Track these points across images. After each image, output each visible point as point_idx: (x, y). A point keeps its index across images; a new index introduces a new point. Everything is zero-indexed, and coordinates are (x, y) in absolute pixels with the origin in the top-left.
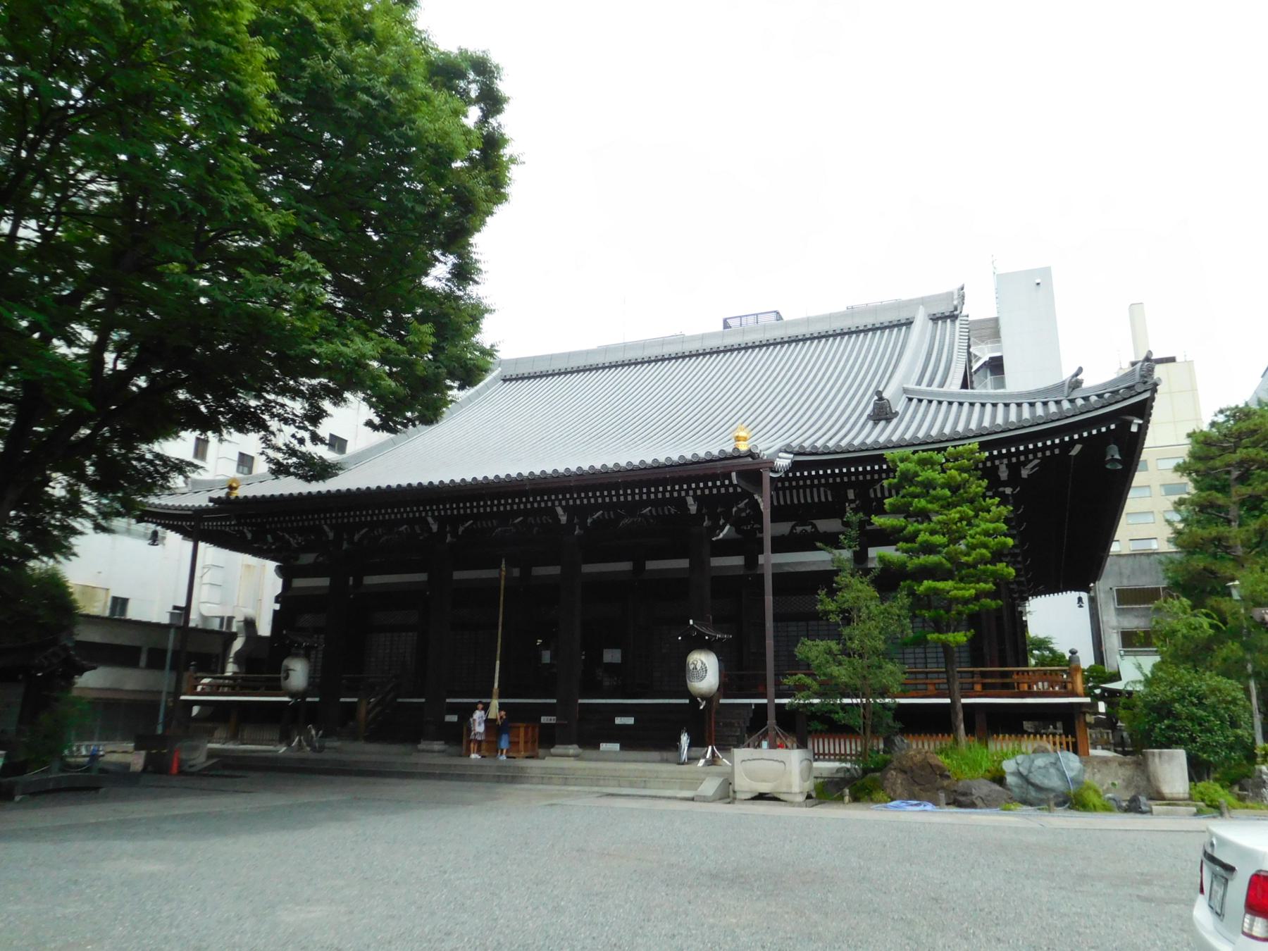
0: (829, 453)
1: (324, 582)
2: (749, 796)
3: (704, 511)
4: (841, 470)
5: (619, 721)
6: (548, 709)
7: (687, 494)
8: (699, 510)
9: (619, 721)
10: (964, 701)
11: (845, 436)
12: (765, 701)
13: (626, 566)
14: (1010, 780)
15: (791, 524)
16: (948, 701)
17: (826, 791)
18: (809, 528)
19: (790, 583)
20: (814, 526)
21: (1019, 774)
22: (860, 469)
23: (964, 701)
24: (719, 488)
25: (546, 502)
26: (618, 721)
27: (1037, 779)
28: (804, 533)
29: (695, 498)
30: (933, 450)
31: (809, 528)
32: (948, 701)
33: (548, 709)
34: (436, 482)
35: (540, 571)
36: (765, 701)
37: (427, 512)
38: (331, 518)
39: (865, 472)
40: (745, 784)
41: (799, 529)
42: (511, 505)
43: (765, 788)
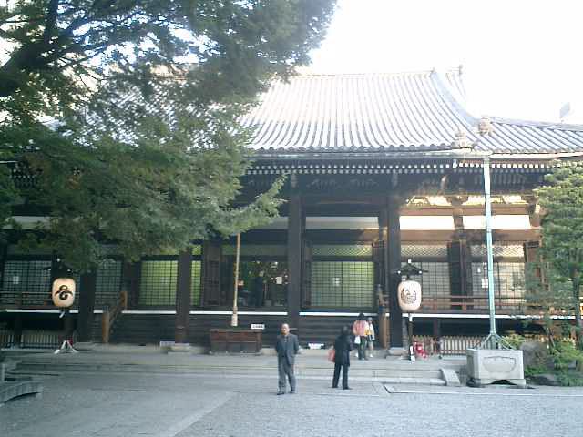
17: (534, 379)
18: (423, 201)
36: (487, 316)
40: (483, 374)
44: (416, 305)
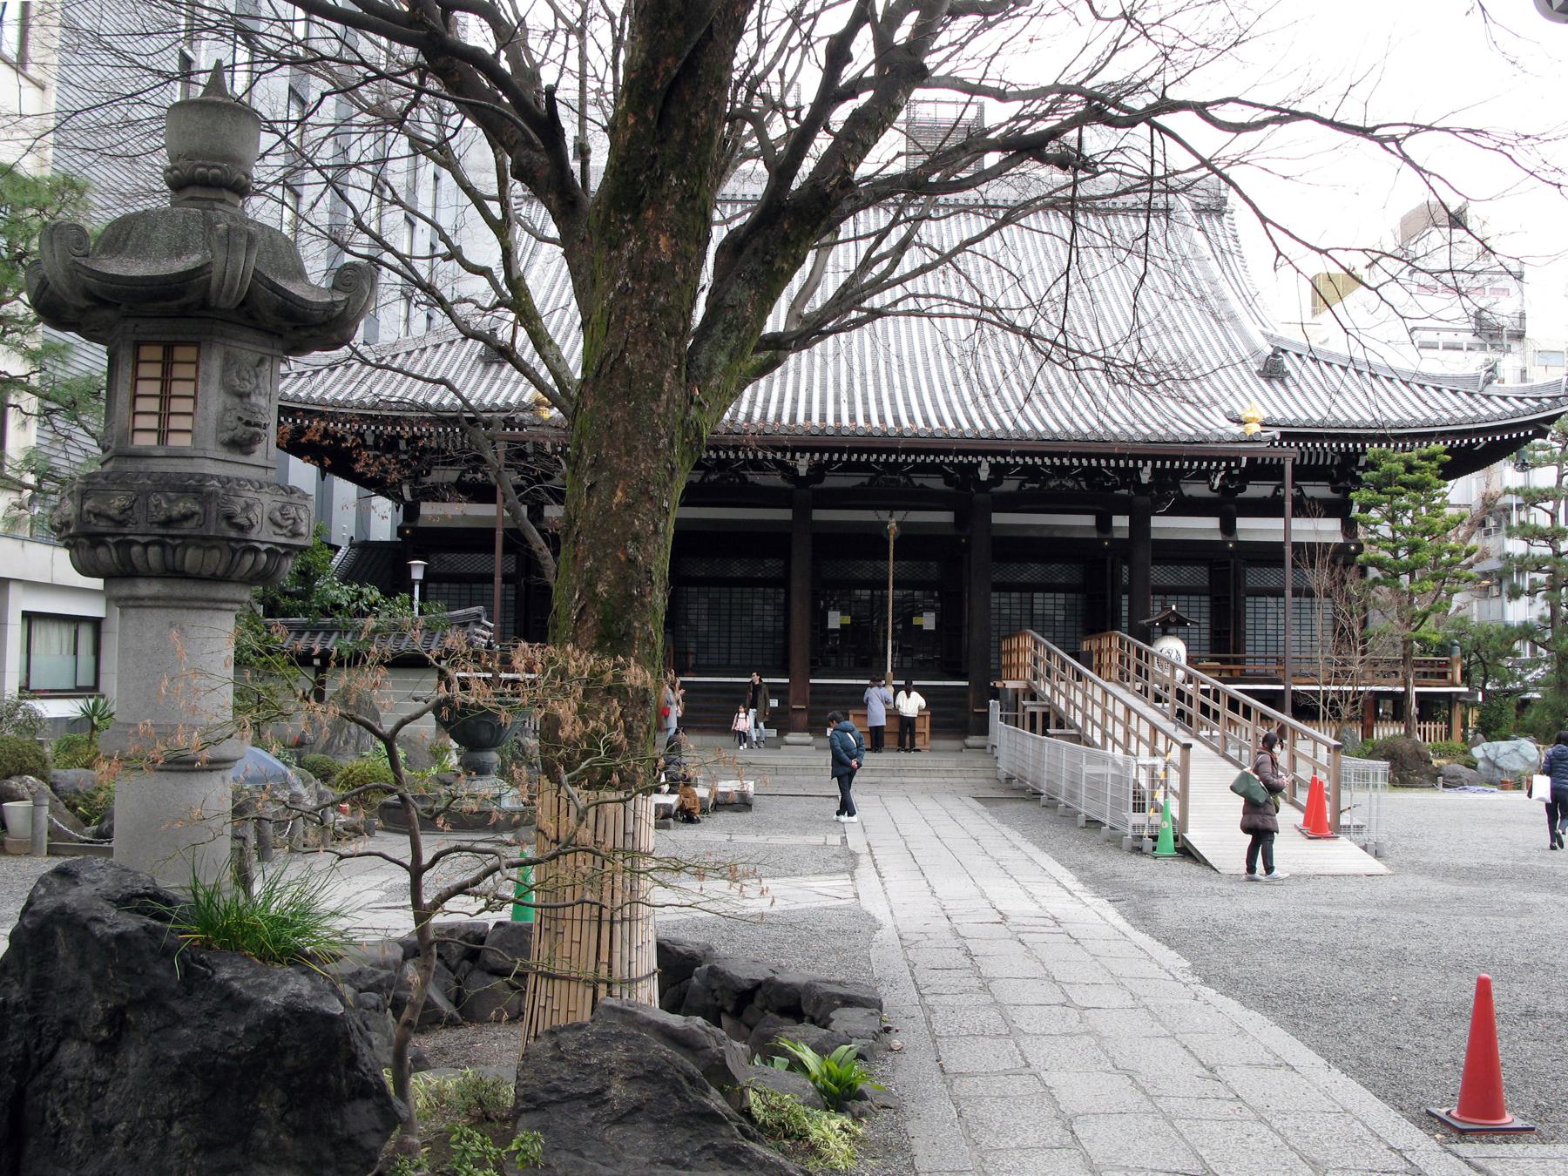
12: (1281, 687)
14: (1481, 765)
19: (1269, 554)
21: (1487, 759)
27: (1502, 763)
36: (1281, 687)
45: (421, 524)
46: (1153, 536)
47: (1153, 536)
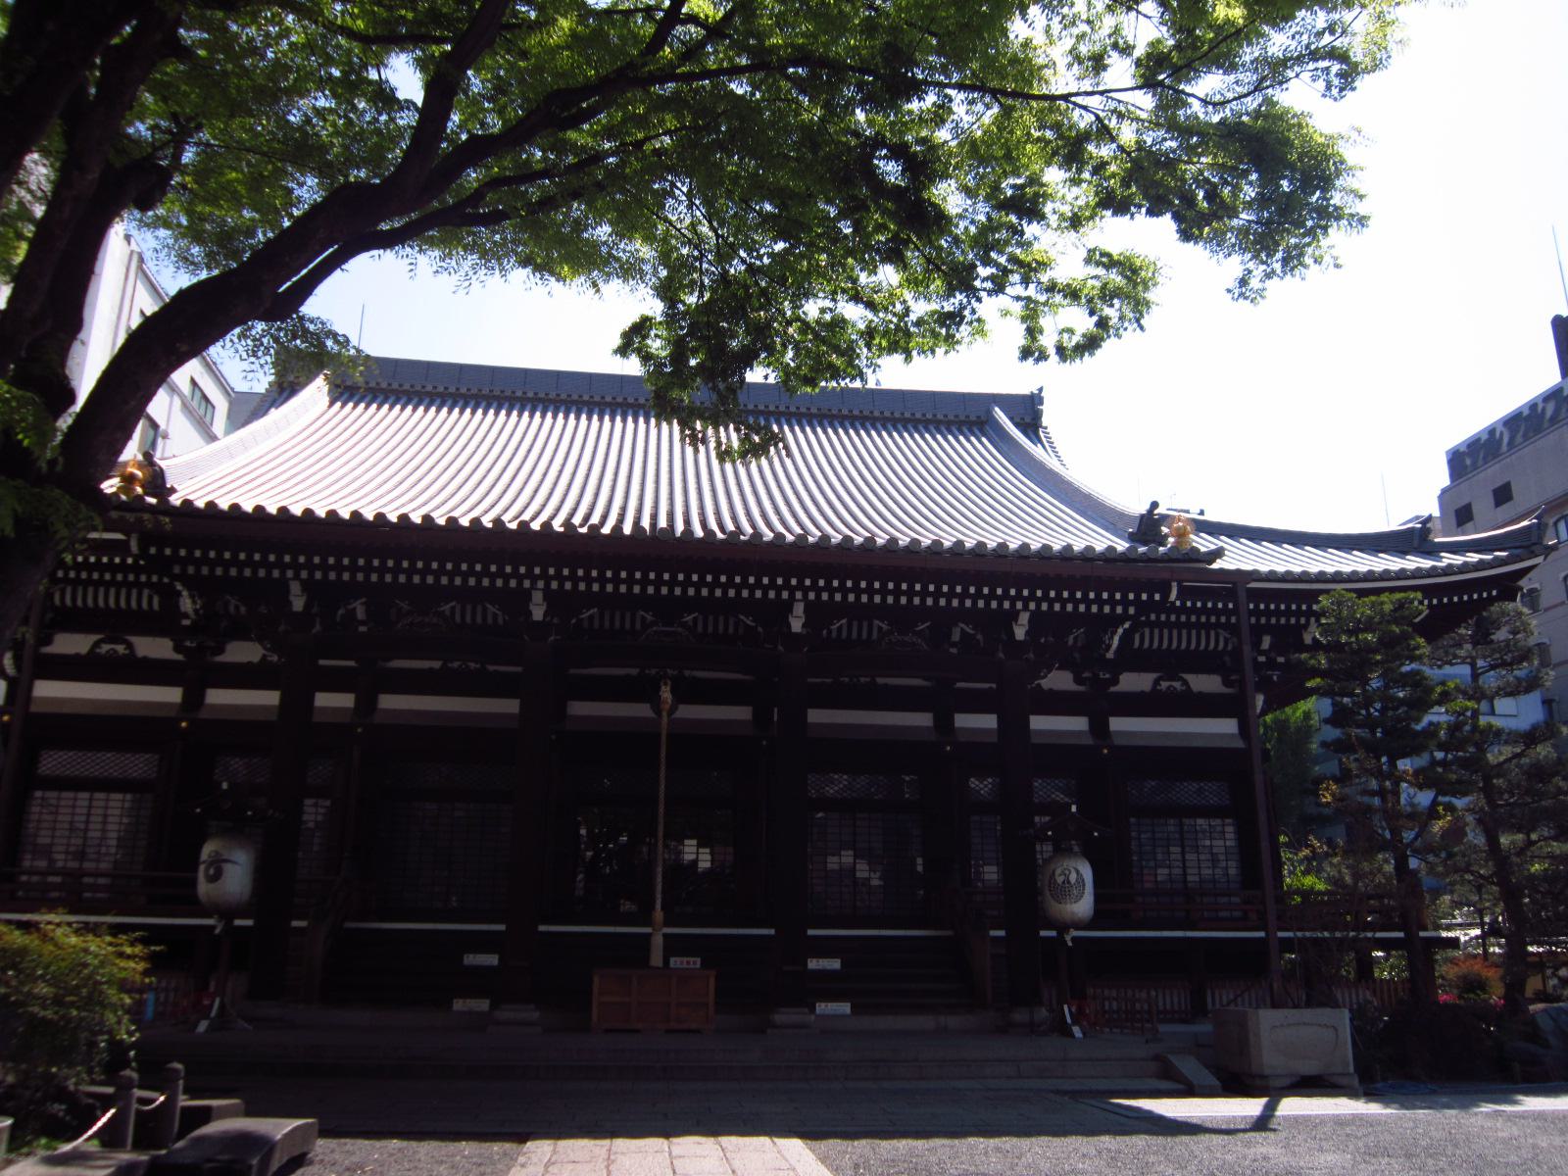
0: (1408, 578)
1: (270, 698)
2: (1286, 1082)
3: (315, 610)
4: (1267, 607)
5: (471, 959)
6: (483, 942)
7: (533, 586)
8: (307, 606)
9: (471, 959)
10: (1281, 934)
11: (431, 499)
13: (923, 720)
15: (1153, 676)
16: (1262, 934)
18: (121, 649)
20: (130, 646)
22: (1272, 607)
23: (1281, 934)
24: (227, 565)
25: (1051, 602)
26: (813, 964)
28: (112, 656)
29: (547, 593)
30: (1414, 588)
31: (1177, 685)
32: (1262, 934)
33: (483, 942)
34: (297, 510)
35: (964, 721)
37: (792, 591)
38: (310, 567)
39: (1288, 613)
41: (1164, 685)
42: (698, 586)
43: (1309, 1068)
44: (1083, 906)
45: (203, 714)
46: (317, 718)
47: (317, 718)
